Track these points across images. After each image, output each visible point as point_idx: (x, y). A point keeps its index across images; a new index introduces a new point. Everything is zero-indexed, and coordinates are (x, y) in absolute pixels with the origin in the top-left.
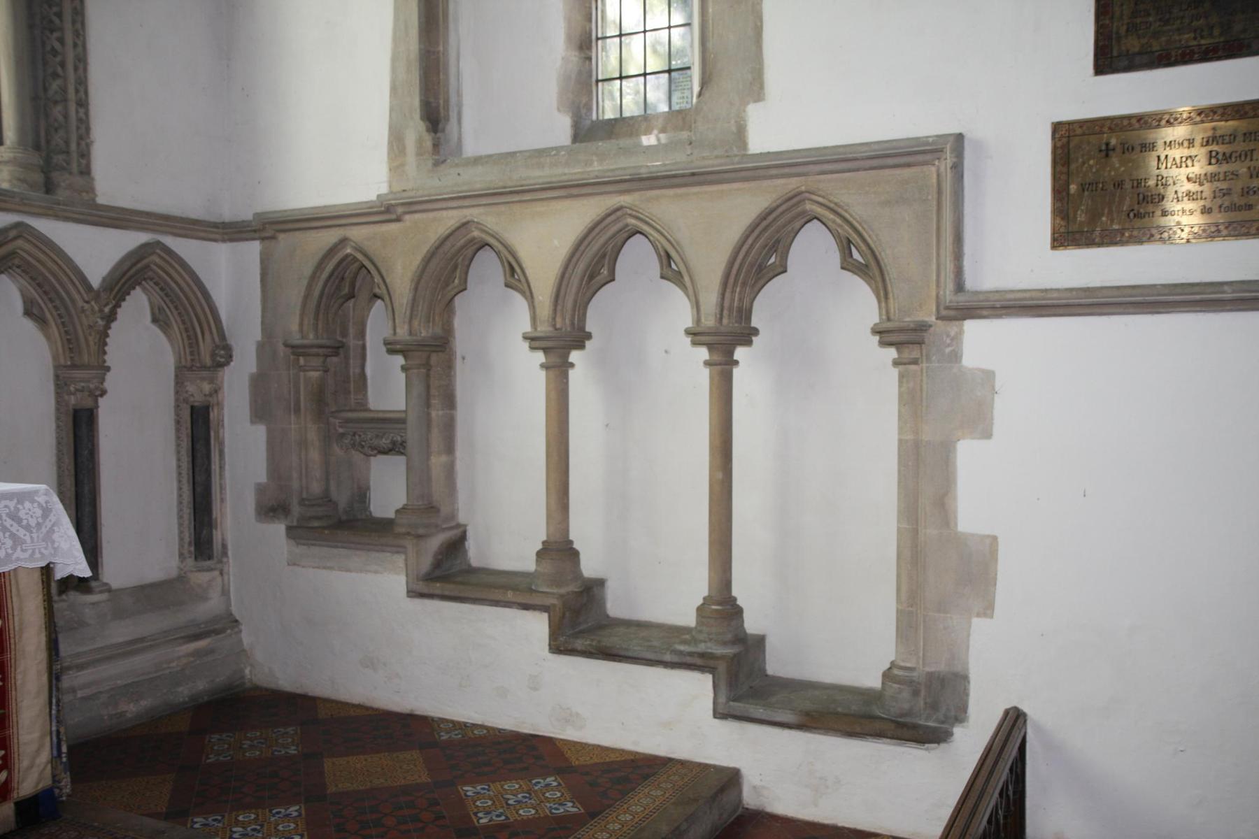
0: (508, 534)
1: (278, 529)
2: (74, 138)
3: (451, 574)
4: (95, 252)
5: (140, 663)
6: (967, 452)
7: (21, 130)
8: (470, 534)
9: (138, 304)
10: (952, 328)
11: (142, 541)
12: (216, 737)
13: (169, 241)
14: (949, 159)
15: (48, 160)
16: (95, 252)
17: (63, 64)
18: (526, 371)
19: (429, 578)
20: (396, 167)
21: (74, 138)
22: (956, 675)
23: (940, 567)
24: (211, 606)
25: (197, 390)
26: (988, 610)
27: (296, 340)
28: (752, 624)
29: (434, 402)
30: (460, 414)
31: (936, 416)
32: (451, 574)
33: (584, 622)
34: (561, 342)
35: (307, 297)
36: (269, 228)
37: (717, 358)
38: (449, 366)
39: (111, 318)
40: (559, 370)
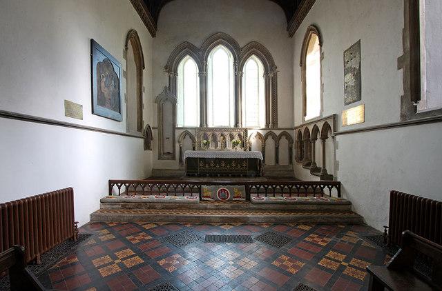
4: (278, 133)
16: (278, 133)
36: (295, 128)
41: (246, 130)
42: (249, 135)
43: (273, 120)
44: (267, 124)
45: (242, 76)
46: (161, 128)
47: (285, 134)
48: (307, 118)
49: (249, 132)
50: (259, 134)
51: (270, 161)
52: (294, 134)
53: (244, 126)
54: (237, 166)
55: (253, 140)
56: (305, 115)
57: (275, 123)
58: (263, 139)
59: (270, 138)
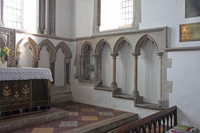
0: (109, 82)
1: (77, 80)
2: (53, 28)
3: (100, 86)
4: (55, 43)
5: (59, 96)
6: (168, 70)
7: (48, 27)
8: (103, 81)
9: (60, 50)
10: (166, 53)
11: (60, 81)
12: (62, 122)
13: (64, 41)
14: (165, 30)
15: (50, 31)
16: (55, 43)
17: (52, 19)
18: (111, 58)
19: (98, 86)
20: (94, 32)
21: (53, 28)
22: (167, 101)
23: (166, 86)
24: (68, 90)
25: (67, 61)
26: (171, 92)
27: (80, 54)
28: (141, 95)
29: (99, 63)
30: (102, 65)
31: (166, 65)
32: (100, 86)
33: (117, 93)
34: (115, 55)
35: (82, 49)
36: (77, 40)
37: (135, 57)
38: (101, 59)
39: (57, 51)
40: (115, 59)
41: (13, 33)
43: (50, 23)
44: (41, 29)
46: (12, 57)
47: (63, 46)
48: (102, 28)
49: (18, 37)
50: (30, 39)
52: (75, 49)
54: (13, 93)
56: (99, 24)
57: (52, 30)
59: (44, 49)
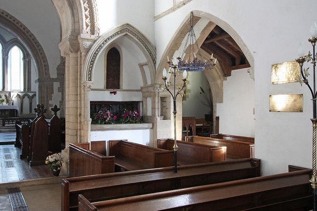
4: (31, 94)
16: (31, 94)
42: (11, 96)
43: (28, 86)
45: (7, 58)
51: (26, 111)
53: (9, 90)
55: (14, 97)
58: (21, 98)
